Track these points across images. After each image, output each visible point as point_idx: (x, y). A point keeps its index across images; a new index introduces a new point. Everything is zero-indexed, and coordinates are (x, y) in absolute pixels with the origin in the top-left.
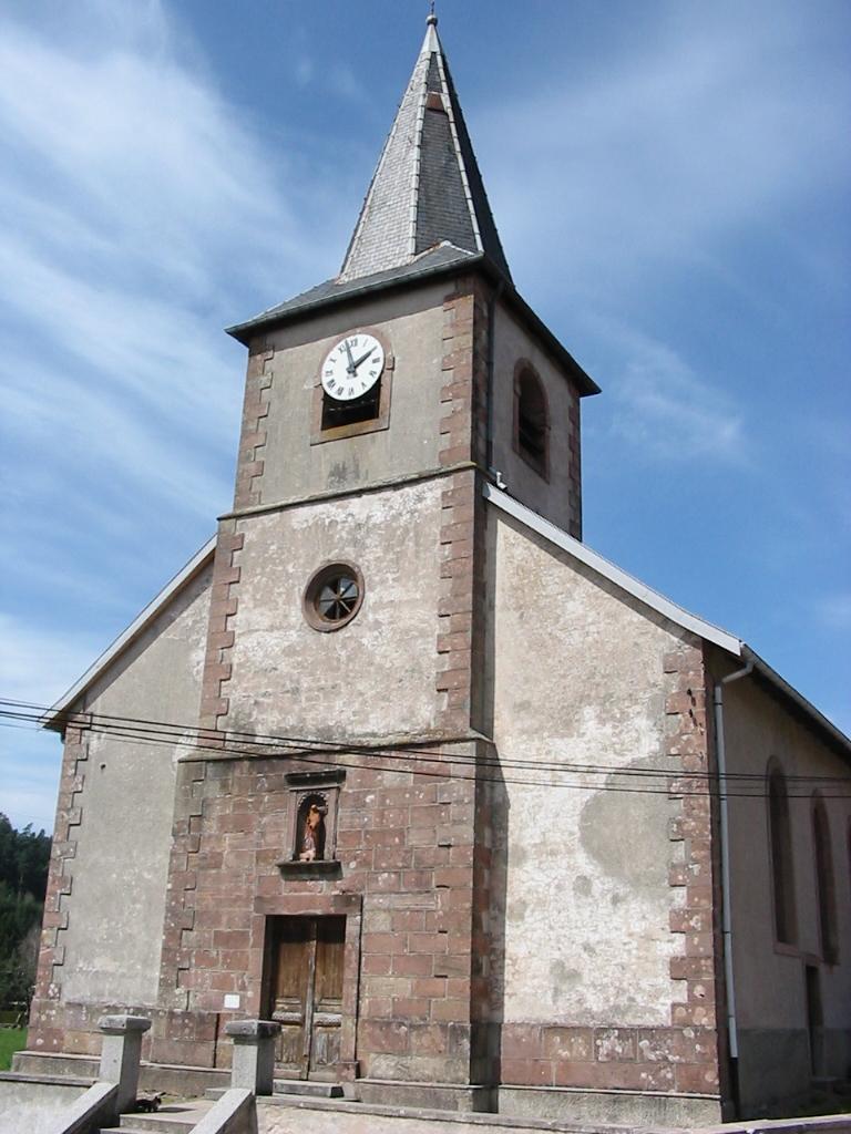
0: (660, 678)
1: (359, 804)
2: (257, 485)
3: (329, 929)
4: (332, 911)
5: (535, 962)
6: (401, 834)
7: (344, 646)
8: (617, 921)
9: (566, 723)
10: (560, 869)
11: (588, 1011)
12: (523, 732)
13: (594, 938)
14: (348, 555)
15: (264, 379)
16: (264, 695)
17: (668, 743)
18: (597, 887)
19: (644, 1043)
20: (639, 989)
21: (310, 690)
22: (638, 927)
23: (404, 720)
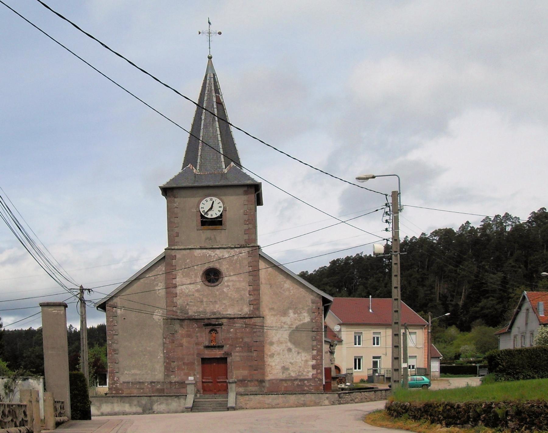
0: (311, 305)
1: (228, 332)
2: (177, 239)
3: (223, 360)
4: (223, 356)
5: (277, 367)
6: (242, 338)
7: (217, 291)
8: (299, 357)
9: (285, 313)
10: (283, 346)
11: (292, 376)
12: (272, 315)
13: (292, 361)
14: (217, 266)
15: (175, 205)
16: (191, 302)
17: (312, 319)
18: (293, 350)
19: (306, 382)
20: (304, 371)
21: (206, 301)
22: (304, 359)
23: (240, 311)
